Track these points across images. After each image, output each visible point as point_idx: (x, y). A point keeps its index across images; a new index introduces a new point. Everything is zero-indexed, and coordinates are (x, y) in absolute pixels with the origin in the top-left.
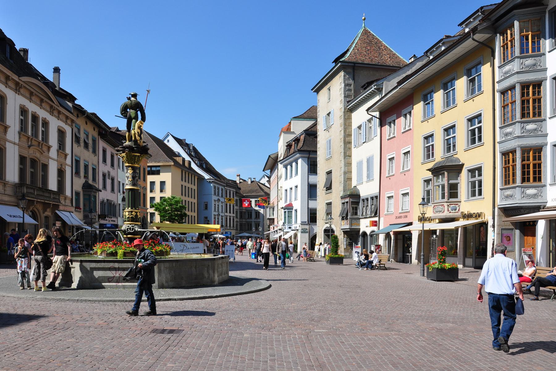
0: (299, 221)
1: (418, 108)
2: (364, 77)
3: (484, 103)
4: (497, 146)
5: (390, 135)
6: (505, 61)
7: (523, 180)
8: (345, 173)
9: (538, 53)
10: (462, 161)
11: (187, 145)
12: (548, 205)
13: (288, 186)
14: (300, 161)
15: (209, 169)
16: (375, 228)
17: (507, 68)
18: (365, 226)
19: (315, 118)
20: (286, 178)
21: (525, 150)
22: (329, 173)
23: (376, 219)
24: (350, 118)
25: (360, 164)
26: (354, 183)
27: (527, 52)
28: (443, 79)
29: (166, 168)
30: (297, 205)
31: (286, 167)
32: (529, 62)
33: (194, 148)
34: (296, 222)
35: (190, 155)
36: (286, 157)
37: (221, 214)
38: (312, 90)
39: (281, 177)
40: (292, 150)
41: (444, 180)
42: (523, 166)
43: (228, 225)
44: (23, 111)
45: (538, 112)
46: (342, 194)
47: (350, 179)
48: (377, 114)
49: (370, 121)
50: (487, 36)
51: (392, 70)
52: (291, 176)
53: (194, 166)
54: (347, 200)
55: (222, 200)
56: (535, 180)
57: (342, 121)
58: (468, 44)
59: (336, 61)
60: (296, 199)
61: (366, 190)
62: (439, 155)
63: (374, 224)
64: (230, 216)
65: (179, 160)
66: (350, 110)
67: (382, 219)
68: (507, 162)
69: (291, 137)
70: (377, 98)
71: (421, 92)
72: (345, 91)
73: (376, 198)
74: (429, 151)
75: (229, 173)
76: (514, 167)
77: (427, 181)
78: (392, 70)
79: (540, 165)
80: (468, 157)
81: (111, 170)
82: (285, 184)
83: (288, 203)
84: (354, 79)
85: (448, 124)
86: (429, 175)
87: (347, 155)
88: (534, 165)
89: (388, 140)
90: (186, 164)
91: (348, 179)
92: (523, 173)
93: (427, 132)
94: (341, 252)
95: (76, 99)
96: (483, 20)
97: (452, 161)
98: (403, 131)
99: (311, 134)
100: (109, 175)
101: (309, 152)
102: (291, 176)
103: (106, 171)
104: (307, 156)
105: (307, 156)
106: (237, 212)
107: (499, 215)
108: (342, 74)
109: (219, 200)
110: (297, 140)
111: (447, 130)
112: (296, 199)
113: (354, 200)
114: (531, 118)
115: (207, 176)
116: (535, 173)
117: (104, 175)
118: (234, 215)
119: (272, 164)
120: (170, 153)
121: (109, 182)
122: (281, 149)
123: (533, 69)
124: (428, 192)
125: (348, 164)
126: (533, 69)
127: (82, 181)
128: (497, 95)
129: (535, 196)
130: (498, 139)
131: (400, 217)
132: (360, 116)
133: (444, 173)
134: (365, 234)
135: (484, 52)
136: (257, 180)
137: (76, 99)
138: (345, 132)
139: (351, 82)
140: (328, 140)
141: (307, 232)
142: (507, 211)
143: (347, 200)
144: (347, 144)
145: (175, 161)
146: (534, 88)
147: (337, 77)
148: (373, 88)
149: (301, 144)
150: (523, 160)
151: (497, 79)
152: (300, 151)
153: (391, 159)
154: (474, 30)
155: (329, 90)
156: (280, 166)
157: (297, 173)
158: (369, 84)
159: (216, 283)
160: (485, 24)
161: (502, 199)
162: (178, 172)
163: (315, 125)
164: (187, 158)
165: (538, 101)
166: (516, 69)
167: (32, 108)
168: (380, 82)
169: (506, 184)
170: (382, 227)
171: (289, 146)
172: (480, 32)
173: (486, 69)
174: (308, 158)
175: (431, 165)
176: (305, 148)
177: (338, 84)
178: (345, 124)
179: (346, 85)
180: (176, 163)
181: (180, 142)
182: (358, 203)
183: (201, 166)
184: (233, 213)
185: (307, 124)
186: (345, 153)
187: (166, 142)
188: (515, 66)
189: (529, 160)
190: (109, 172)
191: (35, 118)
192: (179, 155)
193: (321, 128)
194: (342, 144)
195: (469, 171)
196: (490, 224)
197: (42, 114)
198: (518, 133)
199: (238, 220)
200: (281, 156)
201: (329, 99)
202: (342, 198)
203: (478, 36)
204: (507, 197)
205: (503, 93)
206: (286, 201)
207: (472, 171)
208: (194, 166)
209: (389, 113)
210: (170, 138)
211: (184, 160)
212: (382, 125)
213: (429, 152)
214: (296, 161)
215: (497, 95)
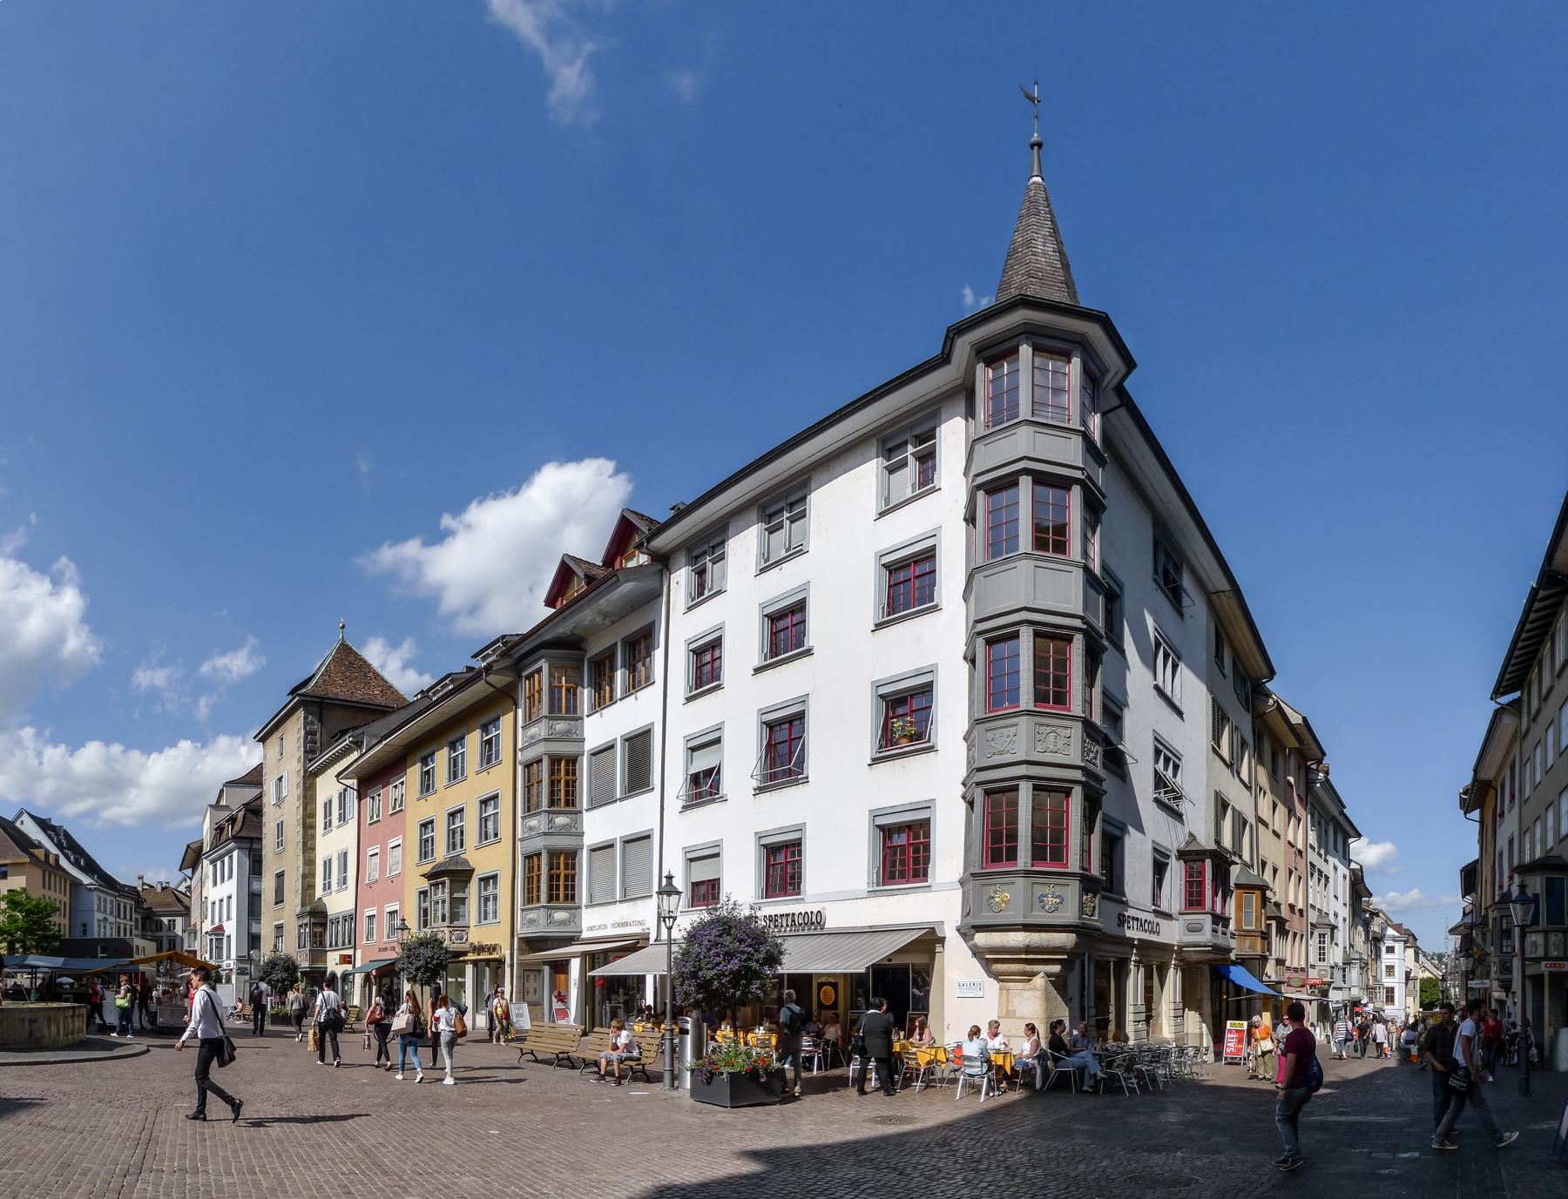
0: (233, 956)
1: (414, 772)
2: (336, 720)
3: (501, 779)
4: (519, 844)
6: (530, 721)
7: (550, 899)
8: (304, 876)
9: (572, 713)
10: (473, 865)
11: (53, 828)
12: (584, 935)
13: (219, 892)
14: (235, 853)
15: (91, 867)
16: (349, 967)
17: (533, 730)
18: (333, 963)
19: (260, 784)
20: (215, 884)
21: (554, 854)
22: (280, 876)
23: (350, 952)
25: (328, 864)
26: (319, 892)
27: (560, 711)
28: (448, 731)
29: (18, 867)
30: (230, 928)
31: (213, 862)
32: (560, 726)
33: (67, 835)
34: (229, 957)
35: (59, 846)
37: (111, 919)
40: (224, 837)
41: (443, 894)
42: (551, 878)
45: (571, 801)
47: (313, 887)
48: (353, 782)
50: (507, 679)
51: (377, 712)
53: (64, 862)
54: (306, 920)
55: (111, 919)
56: (566, 899)
57: (300, 791)
58: (479, 689)
59: (293, 692)
60: (229, 918)
61: (338, 903)
62: (441, 853)
63: (346, 960)
65: (40, 853)
66: (310, 778)
67: (359, 953)
68: (531, 869)
69: (225, 814)
70: (355, 755)
71: (418, 749)
72: (305, 743)
73: (351, 918)
74: (455, 765)
75: (124, 874)
76: (539, 876)
77: (424, 893)
78: (377, 712)
79: (573, 877)
80: (483, 859)
82: (213, 893)
84: (320, 720)
85: (453, 807)
86: (425, 884)
87: (308, 847)
88: (566, 877)
90: (52, 860)
91: (308, 887)
92: (550, 888)
93: (424, 818)
96: (502, 655)
97: (457, 863)
99: (254, 810)
101: (251, 840)
107: (520, 949)
108: (301, 713)
110: (233, 820)
111: (452, 815)
112: (229, 918)
113: (317, 917)
114: (562, 807)
115: (86, 880)
116: (566, 887)
119: (193, 858)
120: (24, 843)
122: (206, 833)
123: (565, 737)
124: (426, 911)
125: (310, 862)
126: (565, 737)
128: (520, 768)
129: (563, 923)
130: (519, 835)
131: (385, 949)
132: (328, 787)
133: (443, 883)
134: (334, 975)
135: (504, 698)
136: (172, 885)
138: (305, 809)
139: (317, 727)
140: (281, 812)
142: (533, 944)
143: (306, 920)
144: (308, 828)
145: (32, 855)
146: (567, 764)
147: (293, 719)
148: (347, 740)
149: (238, 826)
150: (551, 868)
151: (520, 746)
152: (234, 838)
154: (488, 669)
156: (206, 862)
157: (230, 877)
158: (344, 732)
160: (503, 664)
161: (523, 925)
162: (38, 873)
163: (260, 797)
164: (54, 850)
165: (571, 785)
166: (543, 735)
168: (358, 732)
170: (358, 964)
171: (220, 829)
172: (497, 672)
173: (506, 721)
174: (250, 849)
175: (427, 868)
176: (244, 834)
177: (294, 732)
178: (305, 796)
179: (307, 734)
180: (34, 860)
181: (44, 825)
182: (324, 925)
183: (76, 864)
185: (249, 794)
186: (304, 844)
187: (18, 824)
188: (540, 730)
192: (39, 846)
193: (269, 799)
194: (300, 828)
195: (481, 880)
196: (508, 961)
198: (544, 828)
202: (300, 916)
203: (492, 678)
204: (531, 922)
205: (528, 766)
207: (485, 880)
208: (64, 862)
209: (371, 779)
210: (25, 817)
211: (47, 853)
212: (360, 798)
213: (426, 847)
214: (231, 851)
215: (520, 768)
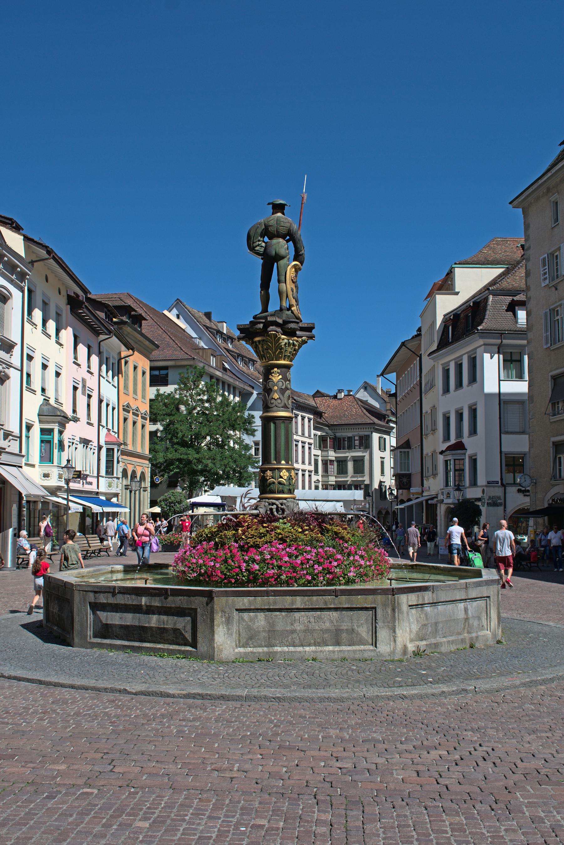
20: (446, 390)
38: (510, 203)
39: (432, 385)
52: (459, 384)
60: (473, 431)
64: (304, 471)
83: (453, 441)
94: (134, 534)
100: (84, 386)
102: (459, 384)
104: (499, 341)
105: (499, 341)
106: (316, 462)
118: (312, 468)
121: (82, 400)
127: (39, 399)
141: (500, 505)
169: (504, 402)
184: (310, 463)
190: (84, 380)
199: (320, 478)
201: (557, 220)
206: (447, 437)
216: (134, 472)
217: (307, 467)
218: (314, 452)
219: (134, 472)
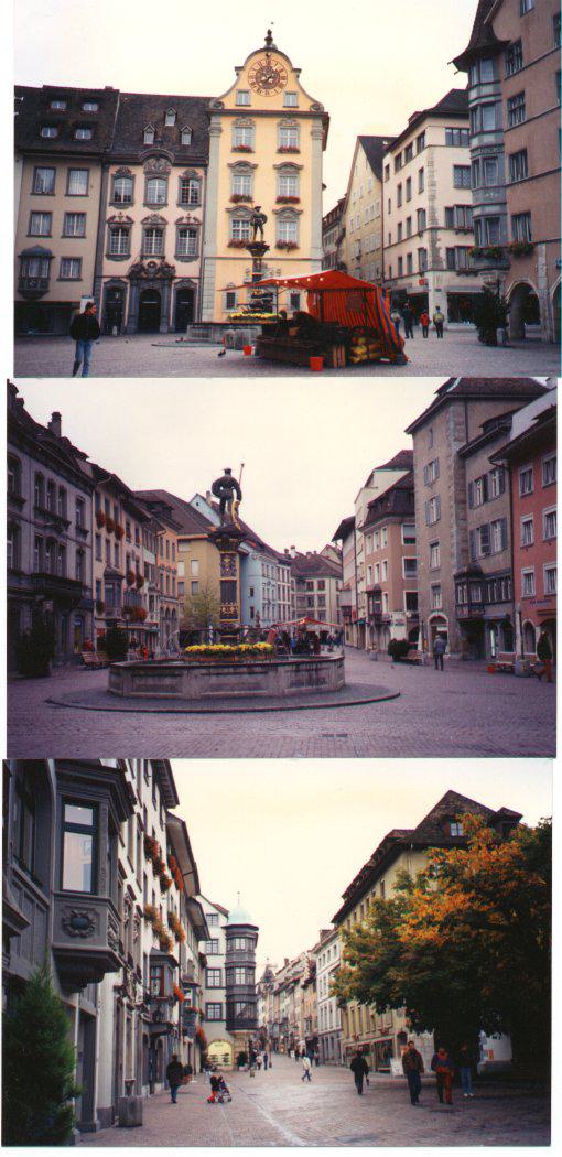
5: (523, 491)
24: (463, 467)
36: (369, 522)
43: (142, 763)
44: (39, 478)
46: (455, 572)
49: (492, 472)
64: (284, 587)
81: (135, 548)
89: (523, 497)
95: (520, 816)
98: (543, 485)
103: (130, 551)
109: (269, 583)
117: (128, 557)
137: (520, 816)
153: (527, 524)
155: (431, 431)
159: (435, 133)
163: (410, 476)
167: (48, 474)
189: (313, 606)
191: (51, 485)
197: (59, 481)
200: (359, 522)
202: (456, 577)
216: (168, 609)
217: (286, 602)
218: (291, 592)
219: (168, 609)
